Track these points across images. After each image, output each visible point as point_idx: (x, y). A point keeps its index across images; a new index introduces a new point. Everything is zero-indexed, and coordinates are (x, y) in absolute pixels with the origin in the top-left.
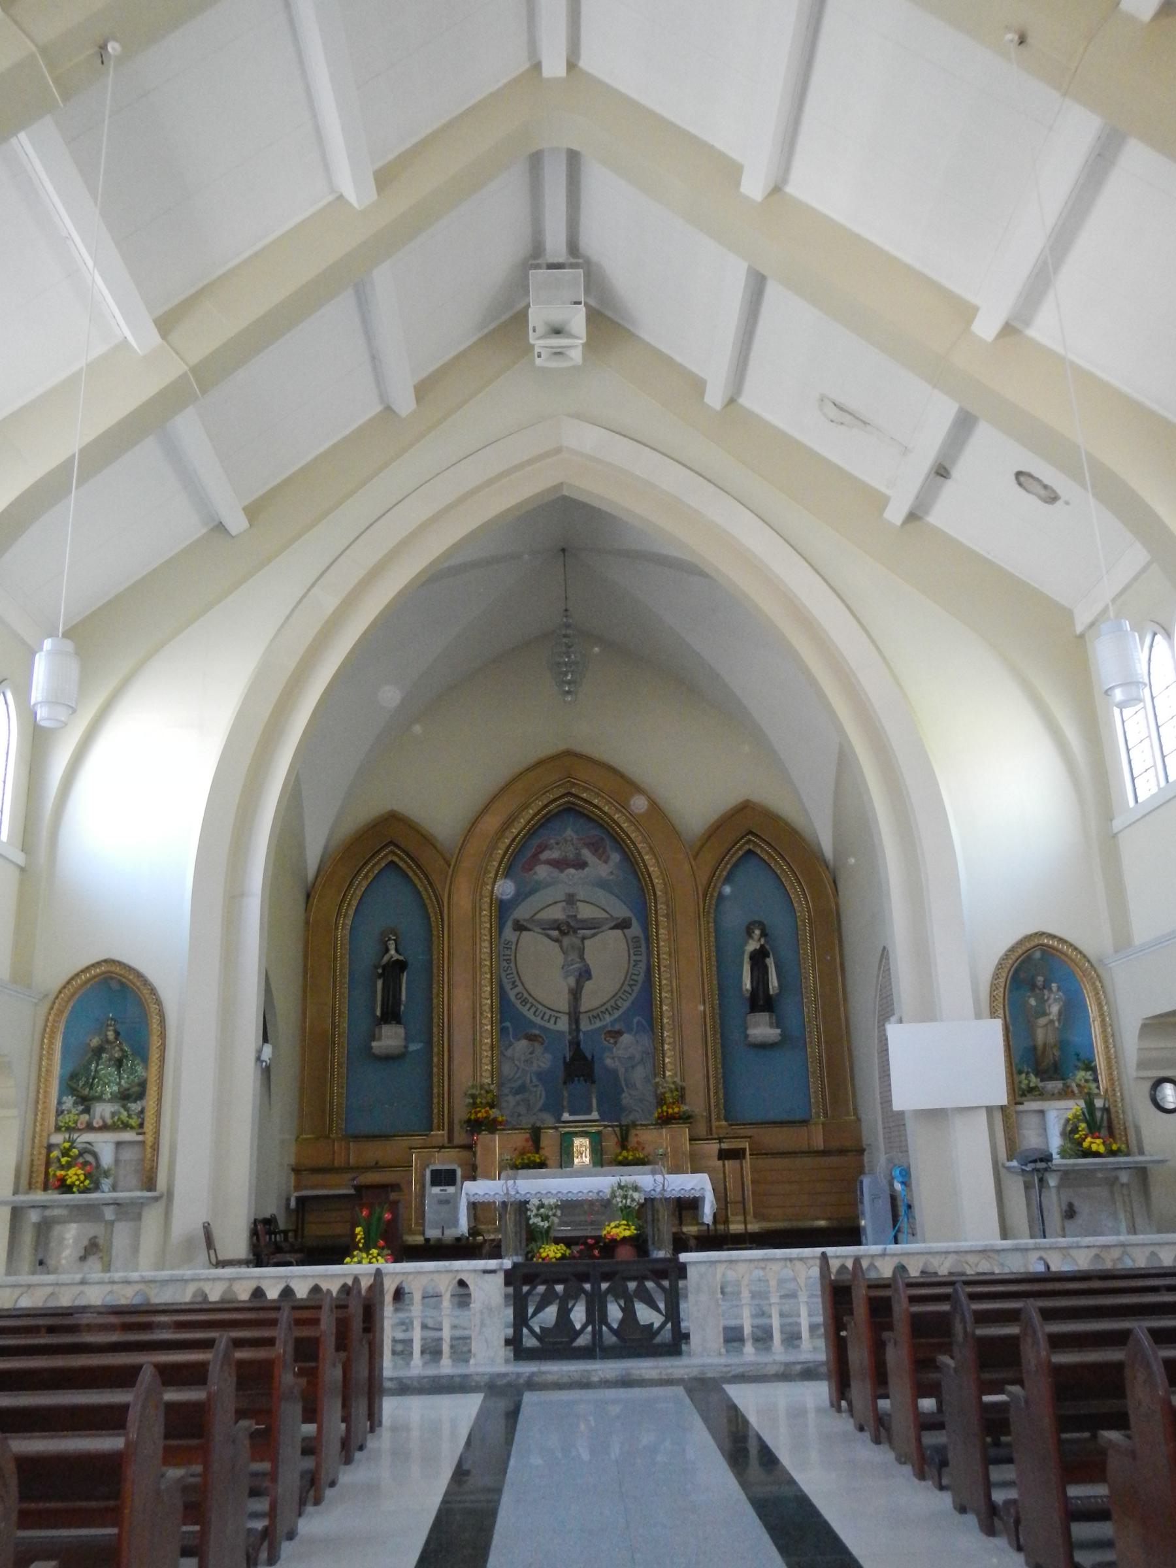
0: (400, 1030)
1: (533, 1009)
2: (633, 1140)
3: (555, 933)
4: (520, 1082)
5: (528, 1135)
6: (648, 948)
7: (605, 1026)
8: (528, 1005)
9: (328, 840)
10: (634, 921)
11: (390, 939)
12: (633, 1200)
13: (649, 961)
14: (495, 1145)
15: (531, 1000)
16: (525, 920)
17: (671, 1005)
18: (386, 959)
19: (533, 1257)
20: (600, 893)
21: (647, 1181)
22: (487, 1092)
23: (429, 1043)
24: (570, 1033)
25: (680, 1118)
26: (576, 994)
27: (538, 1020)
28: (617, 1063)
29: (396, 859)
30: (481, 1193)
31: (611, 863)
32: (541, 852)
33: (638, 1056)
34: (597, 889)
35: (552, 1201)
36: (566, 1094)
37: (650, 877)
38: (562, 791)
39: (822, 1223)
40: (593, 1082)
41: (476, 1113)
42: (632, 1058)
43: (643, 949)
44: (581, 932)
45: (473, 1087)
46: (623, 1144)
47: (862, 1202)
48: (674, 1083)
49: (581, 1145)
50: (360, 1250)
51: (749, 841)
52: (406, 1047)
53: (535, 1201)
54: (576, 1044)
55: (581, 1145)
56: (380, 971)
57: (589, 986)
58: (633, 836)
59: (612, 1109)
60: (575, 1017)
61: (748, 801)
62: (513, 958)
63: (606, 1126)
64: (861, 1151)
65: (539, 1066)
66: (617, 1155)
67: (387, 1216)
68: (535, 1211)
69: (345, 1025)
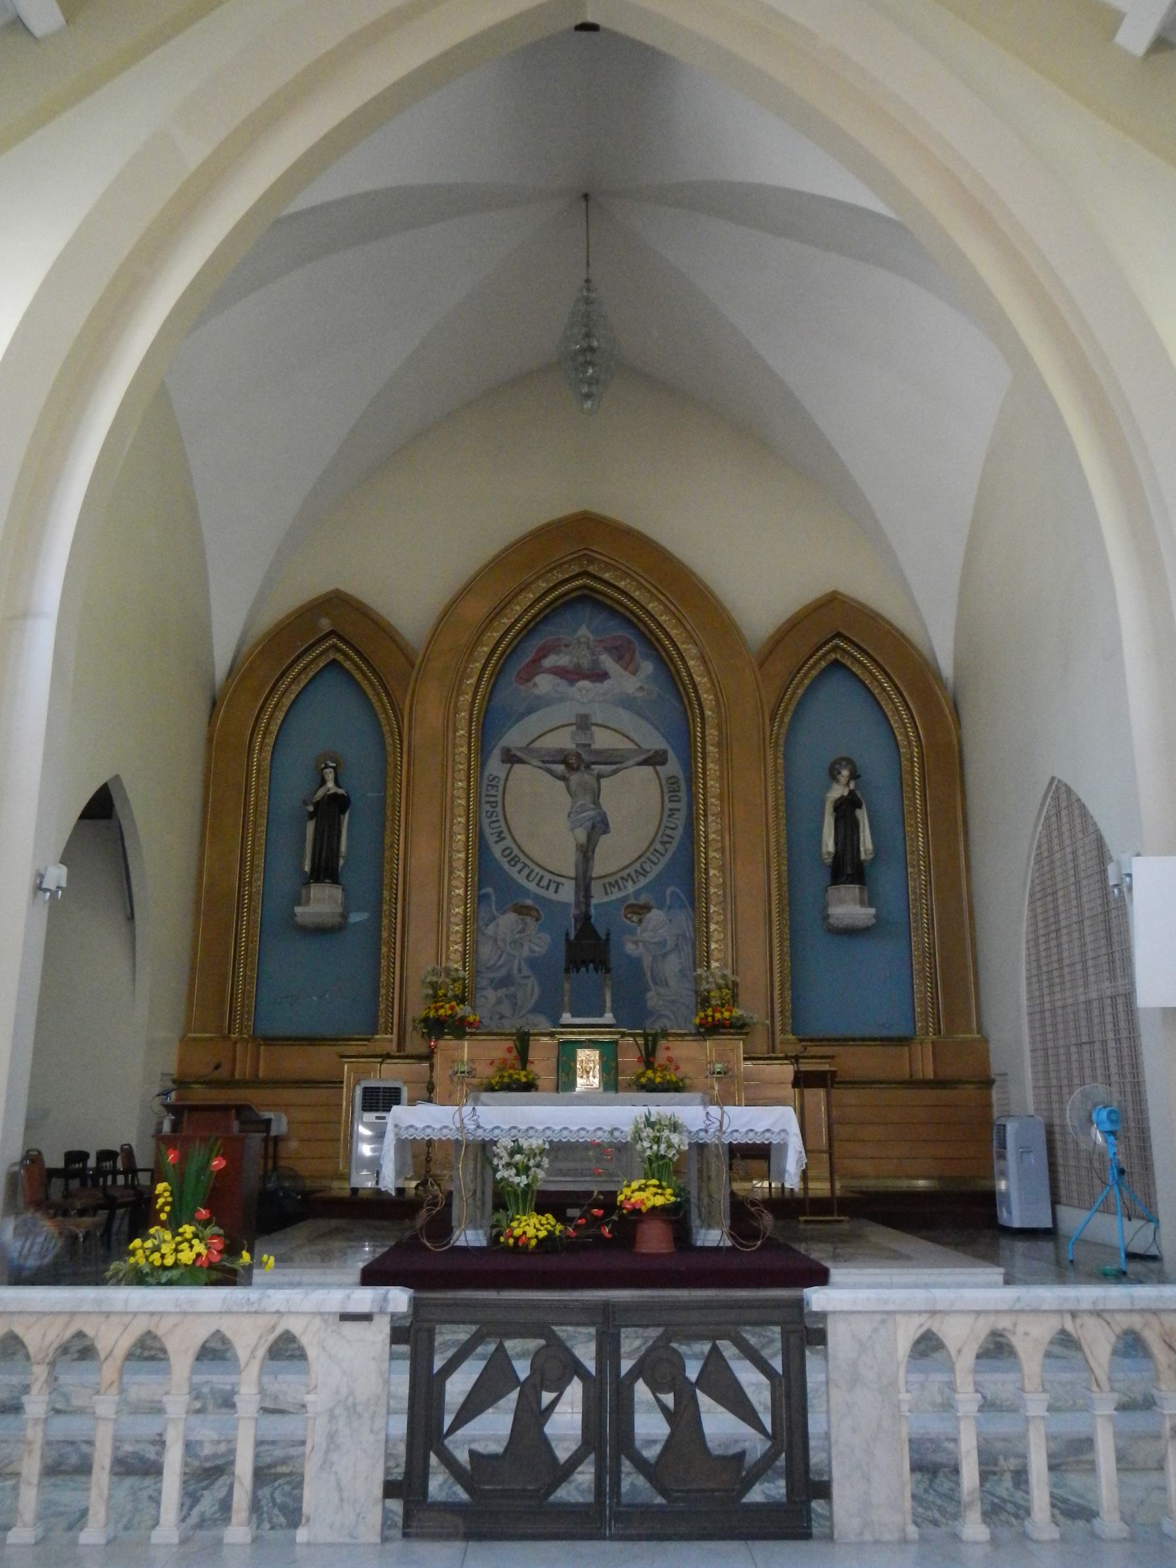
0: (337, 892)
1: (526, 872)
2: (661, 1056)
3: (560, 768)
4: (503, 972)
5: (511, 1044)
6: (689, 789)
7: (626, 897)
8: (519, 866)
9: (245, 633)
10: (671, 755)
11: (327, 767)
12: (670, 1146)
13: (690, 806)
16: (520, 749)
17: (722, 869)
18: (321, 793)
19: (499, 1234)
21: (692, 1115)
22: (455, 981)
23: (377, 912)
24: (577, 904)
26: (586, 853)
27: (532, 886)
28: (641, 949)
29: (340, 657)
31: (642, 675)
32: (545, 656)
33: (670, 943)
34: (621, 711)
35: (536, 1143)
36: (567, 986)
37: (696, 691)
38: (576, 569)
40: (608, 970)
41: (437, 1010)
42: (662, 943)
43: (683, 794)
45: (434, 972)
46: (648, 1059)
47: (1002, 1156)
48: (724, 977)
49: (587, 1057)
50: (163, 1225)
51: (836, 648)
52: (344, 916)
53: (506, 1142)
54: (585, 920)
55: (587, 1057)
56: (311, 808)
57: (605, 844)
58: (673, 633)
59: (633, 1012)
62: (499, 799)
63: (623, 1035)
64: (988, 1083)
65: (532, 951)
66: (639, 1077)
67: (218, 1163)
68: (506, 1159)
69: (260, 883)
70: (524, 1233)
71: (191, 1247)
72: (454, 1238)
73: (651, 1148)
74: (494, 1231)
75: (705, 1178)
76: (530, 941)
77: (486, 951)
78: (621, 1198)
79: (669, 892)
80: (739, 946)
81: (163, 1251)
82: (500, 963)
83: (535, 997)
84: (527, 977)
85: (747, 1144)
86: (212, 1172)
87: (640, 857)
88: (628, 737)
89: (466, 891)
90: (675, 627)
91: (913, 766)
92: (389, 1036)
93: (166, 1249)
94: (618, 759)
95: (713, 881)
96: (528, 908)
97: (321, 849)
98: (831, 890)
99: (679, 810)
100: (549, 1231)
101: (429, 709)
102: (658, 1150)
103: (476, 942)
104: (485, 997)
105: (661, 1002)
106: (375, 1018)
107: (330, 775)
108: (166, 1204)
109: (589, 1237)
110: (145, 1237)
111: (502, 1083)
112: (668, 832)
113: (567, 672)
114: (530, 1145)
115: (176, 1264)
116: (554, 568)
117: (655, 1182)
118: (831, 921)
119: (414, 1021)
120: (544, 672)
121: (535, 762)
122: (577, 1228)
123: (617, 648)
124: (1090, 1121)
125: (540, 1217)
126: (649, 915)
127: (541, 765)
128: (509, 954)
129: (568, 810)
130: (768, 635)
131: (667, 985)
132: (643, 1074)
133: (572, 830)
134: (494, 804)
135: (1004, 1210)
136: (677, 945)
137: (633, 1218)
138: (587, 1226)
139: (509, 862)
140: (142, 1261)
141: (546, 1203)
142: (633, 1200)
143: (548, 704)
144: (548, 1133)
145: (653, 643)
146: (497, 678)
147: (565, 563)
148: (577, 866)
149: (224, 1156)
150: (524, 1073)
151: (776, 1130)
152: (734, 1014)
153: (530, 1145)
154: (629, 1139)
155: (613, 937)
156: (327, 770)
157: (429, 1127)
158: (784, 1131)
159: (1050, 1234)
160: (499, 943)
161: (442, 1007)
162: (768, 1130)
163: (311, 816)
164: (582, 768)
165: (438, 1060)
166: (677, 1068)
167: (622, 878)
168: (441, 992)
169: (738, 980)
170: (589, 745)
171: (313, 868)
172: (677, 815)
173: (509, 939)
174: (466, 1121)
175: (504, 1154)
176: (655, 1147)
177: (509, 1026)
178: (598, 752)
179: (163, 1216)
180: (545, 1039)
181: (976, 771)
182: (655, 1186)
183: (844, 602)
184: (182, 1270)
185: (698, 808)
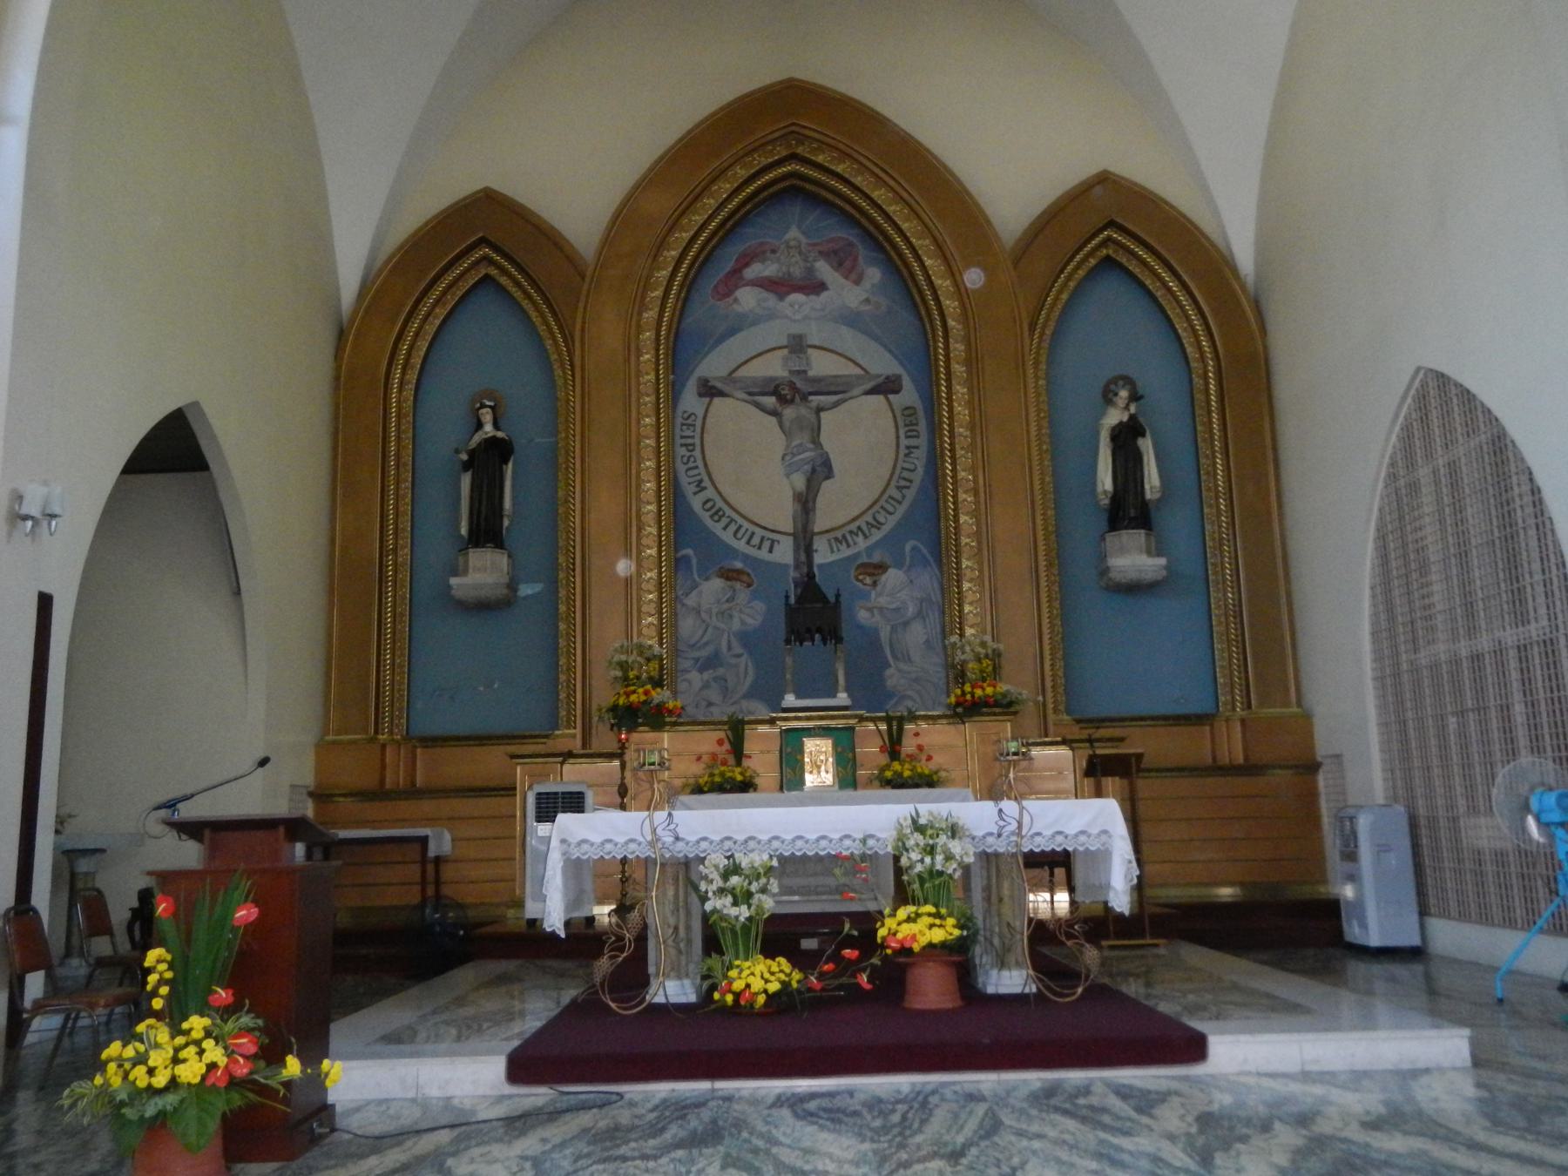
0: (502, 559)
1: (733, 527)
2: (908, 746)
3: (770, 401)
7: (857, 555)
8: (725, 521)
10: (907, 382)
11: (483, 406)
12: (949, 857)
13: (932, 442)
15: (728, 512)
17: (975, 514)
18: (477, 438)
19: (713, 988)
20: (846, 332)
24: (797, 567)
25: (997, 704)
26: (806, 503)
27: (741, 545)
28: (878, 617)
29: (494, 272)
30: (597, 839)
31: (867, 284)
32: (747, 265)
33: (911, 610)
34: (845, 330)
35: (759, 859)
36: (789, 660)
39: (1226, 893)
40: (839, 640)
41: (628, 695)
43: (922, 426)
44: (815, 400)
45: (622, 650)
46: (893, 748)
48: (983, 644)
49: (818, 750)
50: (158, 1015)
52: (512, 586)
55: (818, 750)
56: (464, 457)
59: (871, 694)
60: (804, 540)
62: (697, 441)
63: (862, 719)
64: (1312, 767)
65: (743, 622)
68: (718, 882)
70: (748, 986)
71: (201, 1052)
72: (651, 991)
73: (922, 861)
74: (706, 984)
75: (994, 899)
77: (687, 625)
78: (882, 932)
79: (908, 547)
80: (997, 611)
81: (151, 1063)
82: (705, 639)
83: (750, 679)
85: (1053, 850)
86: (234, 929)
89: (660, 552)
90: (907, 220)
91: (1207, 384)
93: (156, 1059)
95: (965, 529)
96: (739, 572)
98: (1110, 537)
100: (782, 982)
101: (605, 327)
102: (933, 864)
106: (556, 716)
107: (487, 416)
108: (161, 982)
109: (840, 987)
110: (129, 1037)
112: (905, 474)
115: (173, 1083)
116: (754, 150)
117: (930, 908)
118: (1112, 575)
119: (600, 710)
120: (747, 285)
123: (835, 252)
124: (1526, 808)
125: (769, 962)
126: (884, 578)
128: (716, 628)
130: (1018, 234)
132: (888, 767)
133: (788, 476)
134: (690, 447)
135: (1355, 923)
137: (902, 960)
138: (836, 975)
140: (116, 1082)
141: (778, 937)
142: (900, 936)
143: (754, 324)
144: (776, 844)
145: (879, 241)
146: (688, 292)
149: (256, 903)
150: (738, 770)
151: (1095, 831)
156: (484, 411)
158: (1105, 832)
159: (1415, 954)
160: (704, 615)
162: (1083, 832)
163: (466, 466)
164: (797, 399)
165: (630, 755)
166: (929, 758)
168: (631, 674)
169: (1001, 647)
170: (805, 372)
171: (471, 531)
172: (916, 453)
173: (715, 610)
174: (659, 831)
175: (715, 876)
177: (719, 713)
179: (157, 1004)
181: (1290, 385)
182: (930, 915)
183: (1115, 182)
184: (183, 1093)
185: (943, 442)
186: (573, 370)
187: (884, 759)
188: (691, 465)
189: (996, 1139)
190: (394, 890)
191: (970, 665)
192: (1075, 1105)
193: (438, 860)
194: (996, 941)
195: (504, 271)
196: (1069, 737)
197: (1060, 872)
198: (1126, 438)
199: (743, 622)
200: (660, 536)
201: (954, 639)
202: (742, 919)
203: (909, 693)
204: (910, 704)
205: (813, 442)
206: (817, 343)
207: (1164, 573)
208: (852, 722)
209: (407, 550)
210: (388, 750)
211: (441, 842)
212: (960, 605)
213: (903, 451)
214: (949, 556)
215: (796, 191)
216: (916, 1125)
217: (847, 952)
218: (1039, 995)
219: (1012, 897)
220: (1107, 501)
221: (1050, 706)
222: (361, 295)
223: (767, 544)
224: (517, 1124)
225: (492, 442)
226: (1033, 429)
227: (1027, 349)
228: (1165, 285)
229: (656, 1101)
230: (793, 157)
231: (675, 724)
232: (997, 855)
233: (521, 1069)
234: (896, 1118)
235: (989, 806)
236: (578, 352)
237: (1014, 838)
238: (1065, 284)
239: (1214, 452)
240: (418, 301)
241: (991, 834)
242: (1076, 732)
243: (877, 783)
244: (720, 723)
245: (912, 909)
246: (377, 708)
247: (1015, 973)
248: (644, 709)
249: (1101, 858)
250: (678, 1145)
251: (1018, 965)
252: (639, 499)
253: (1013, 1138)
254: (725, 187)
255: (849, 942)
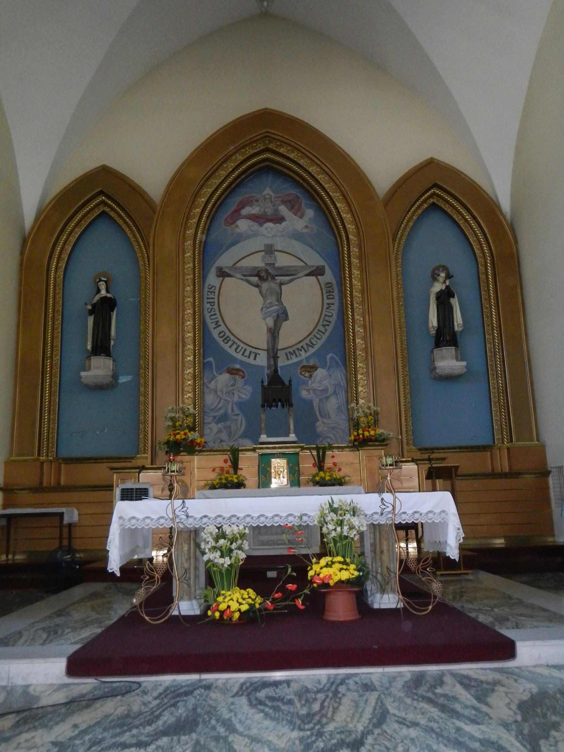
0: (109, 362)
1: (235, 346)
2: (328, 463)
3: (255, 279)
4: (222, 412)
7: (301, 361)
8: (230, 343)
10: (327, 270)
11: (100, 280)
12: (351, 528)
13: (341, 300)
14: (201, 467)
15: (232, 338)
17: (364, 338)
18: (97, 297)
19: (208, 608)
20: (295, 243)
24: (269, 367)
25: (376, 440)
26: (274, 333)
27: (239, 356)
29: (107, 209)
30: (140, 516)
31: (306, 218)
32: (243, 207)
33: (331, 390)
39: (499, 542)
40: (291, 405)
41: (175, 435)
42: (326, 390)
43: (336, 293)
44: (279, 279)
46: (320, 464)
48: (369, 408)
49: (279, 464)
52: (115, 377)
55: (279, 464)
59: (308, 434)
60: (273, 354)
61: (432, 158)
62: (216, 301)
63: (303, 448)
64: (546, 473)
65: (240, 397)
68: (212, 543)
70: (229, 607)
73: (335, 530)
76: (239, 391)
77: (210, 399)
78: (311, 573)
79: (329, 356)
80: (376, 393)
82: (220, 405)
84: (238, 415)
87: (308, 335)
88: (299, 259)
89: (195, 358)
91: (486, 269)
92: (146, 455)
94: (292, 273)
96: (237, 370)
97: (98, 334)
98: (436, 351)
99: (333, 304)
100: (250, 605)
102: (342, 532)
103: (202, 394)
104: (211, 429)
105: (325, 429)
107: (103, 286)
109: (285, 607)
111: (221, 483)
112: (327, 318)
113: (258, 217)
114: (232, 531)
117: (340, 559)
120: (242, 218)
121: (239, 276)
122: (274, 601)
125: (242, 591)
126: (316, 372)
127: (242, 277)
129: (261, 306)
131: (329, 417)
132: (317, 475)
133: (264, 319)
136: (335, 392)
138: (284, 599)
139: (223, 341)
141: (251, 574)
142: (322, 576)
144: (248, 519)
147: (254, 142)
148: (268, 342)
150: (235, 476)
151: (437, 511)
152: (377, 432)
153: (232, 531)
154: (316, 523)
155: (294, 383)
156: (101, 283)
157: (148, 518)
158: (443, 511)
160: (219, 393)
161: (178, 433)
162: (430, 512)
163: (91, 312)
164: (269, 278)
166: (340, 470)
167: (298, 349)
168: (177, 424)
169: (379, 409)
170: (274, 264)
172: (333, 307)
173: (225, 390)
174: (177, 512)
175: (210, 539)
176: (339, 529)
178: (280, 268)
180: (249, 454)
181: (530, 270)
182: (340, 562)
185: (346, 300)
186: (149, 262)
187: (315, 470)
188: (212, 313)
189: (385, 727)
190: (46, 542)
191: (362, 419)
192: (435, 694)
193: (70, 525)
194: (379, 577)
195: (113, 209)
196: (415, 458)
197: (412, 532)
198: (444, 299)
199: (240, 397)
200: (195, 350)
201: (353, 405)
202: (226, 566)
203: (329, 435)
204: (329, 440)
205: (278, 301)
206: (280, 249)
207: (465, 370)
208: (297, 450)
209: (58, 357)
210: (45, 466)
211: (72, 515)
212: (356, 387)
213: (326, 306)
214: (350, 361)
215: (269, 169)
216: (330, 714)
217: (290, 586)
218: (405, 608)
219: (388, 550)
220: (434, 332)
221: (405, 441)
222: (36, 220)
223: (253, 356)
224: (75, 704)
225: (104, 299)
226: (395, 294)
227: (391, 252)
228: (464, 217)
229: (161, 689)
230: (267, 150)
231: (200, 451)
232: (379, 525)
233: (77, 666)
234: (316, 707)
235: (374, 498)
236: (151, 252)
237: (390, 516)
238: (411, 217)
239: (490, 306)
240: (66, 224)
241: (376, 513)
242: (418, 455)
243: (311, 483)
244: (225, 450)
245: (329, 559)
246: (39, 443)
247: (391, 596)
248: (184, 443)
249: (442, 526)
250: (165, 733)
251: (393, 591)
252: (183, 330)
253: (396, 726)
254: (231, 165)
255: (291, 580)
